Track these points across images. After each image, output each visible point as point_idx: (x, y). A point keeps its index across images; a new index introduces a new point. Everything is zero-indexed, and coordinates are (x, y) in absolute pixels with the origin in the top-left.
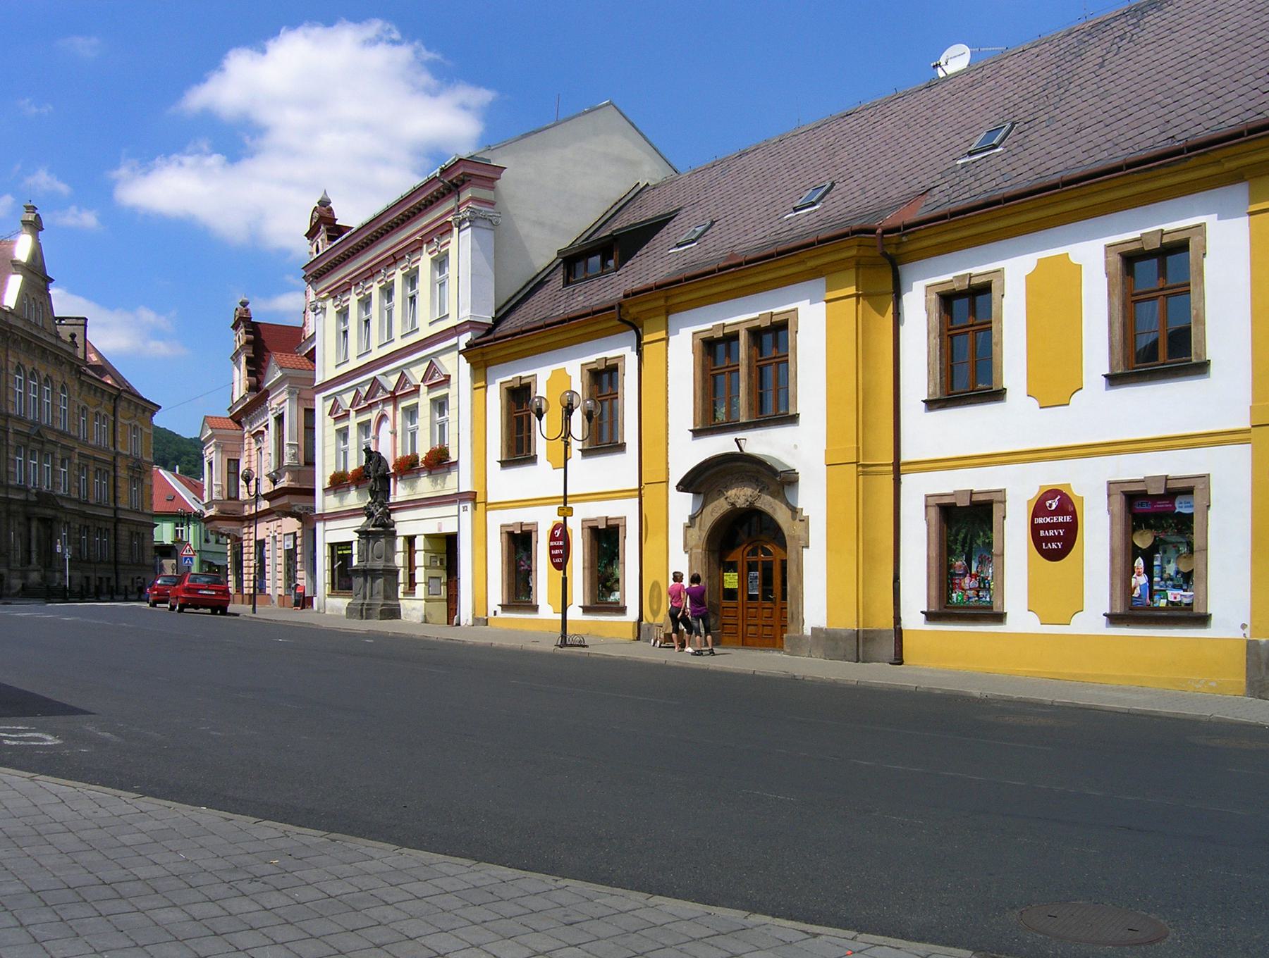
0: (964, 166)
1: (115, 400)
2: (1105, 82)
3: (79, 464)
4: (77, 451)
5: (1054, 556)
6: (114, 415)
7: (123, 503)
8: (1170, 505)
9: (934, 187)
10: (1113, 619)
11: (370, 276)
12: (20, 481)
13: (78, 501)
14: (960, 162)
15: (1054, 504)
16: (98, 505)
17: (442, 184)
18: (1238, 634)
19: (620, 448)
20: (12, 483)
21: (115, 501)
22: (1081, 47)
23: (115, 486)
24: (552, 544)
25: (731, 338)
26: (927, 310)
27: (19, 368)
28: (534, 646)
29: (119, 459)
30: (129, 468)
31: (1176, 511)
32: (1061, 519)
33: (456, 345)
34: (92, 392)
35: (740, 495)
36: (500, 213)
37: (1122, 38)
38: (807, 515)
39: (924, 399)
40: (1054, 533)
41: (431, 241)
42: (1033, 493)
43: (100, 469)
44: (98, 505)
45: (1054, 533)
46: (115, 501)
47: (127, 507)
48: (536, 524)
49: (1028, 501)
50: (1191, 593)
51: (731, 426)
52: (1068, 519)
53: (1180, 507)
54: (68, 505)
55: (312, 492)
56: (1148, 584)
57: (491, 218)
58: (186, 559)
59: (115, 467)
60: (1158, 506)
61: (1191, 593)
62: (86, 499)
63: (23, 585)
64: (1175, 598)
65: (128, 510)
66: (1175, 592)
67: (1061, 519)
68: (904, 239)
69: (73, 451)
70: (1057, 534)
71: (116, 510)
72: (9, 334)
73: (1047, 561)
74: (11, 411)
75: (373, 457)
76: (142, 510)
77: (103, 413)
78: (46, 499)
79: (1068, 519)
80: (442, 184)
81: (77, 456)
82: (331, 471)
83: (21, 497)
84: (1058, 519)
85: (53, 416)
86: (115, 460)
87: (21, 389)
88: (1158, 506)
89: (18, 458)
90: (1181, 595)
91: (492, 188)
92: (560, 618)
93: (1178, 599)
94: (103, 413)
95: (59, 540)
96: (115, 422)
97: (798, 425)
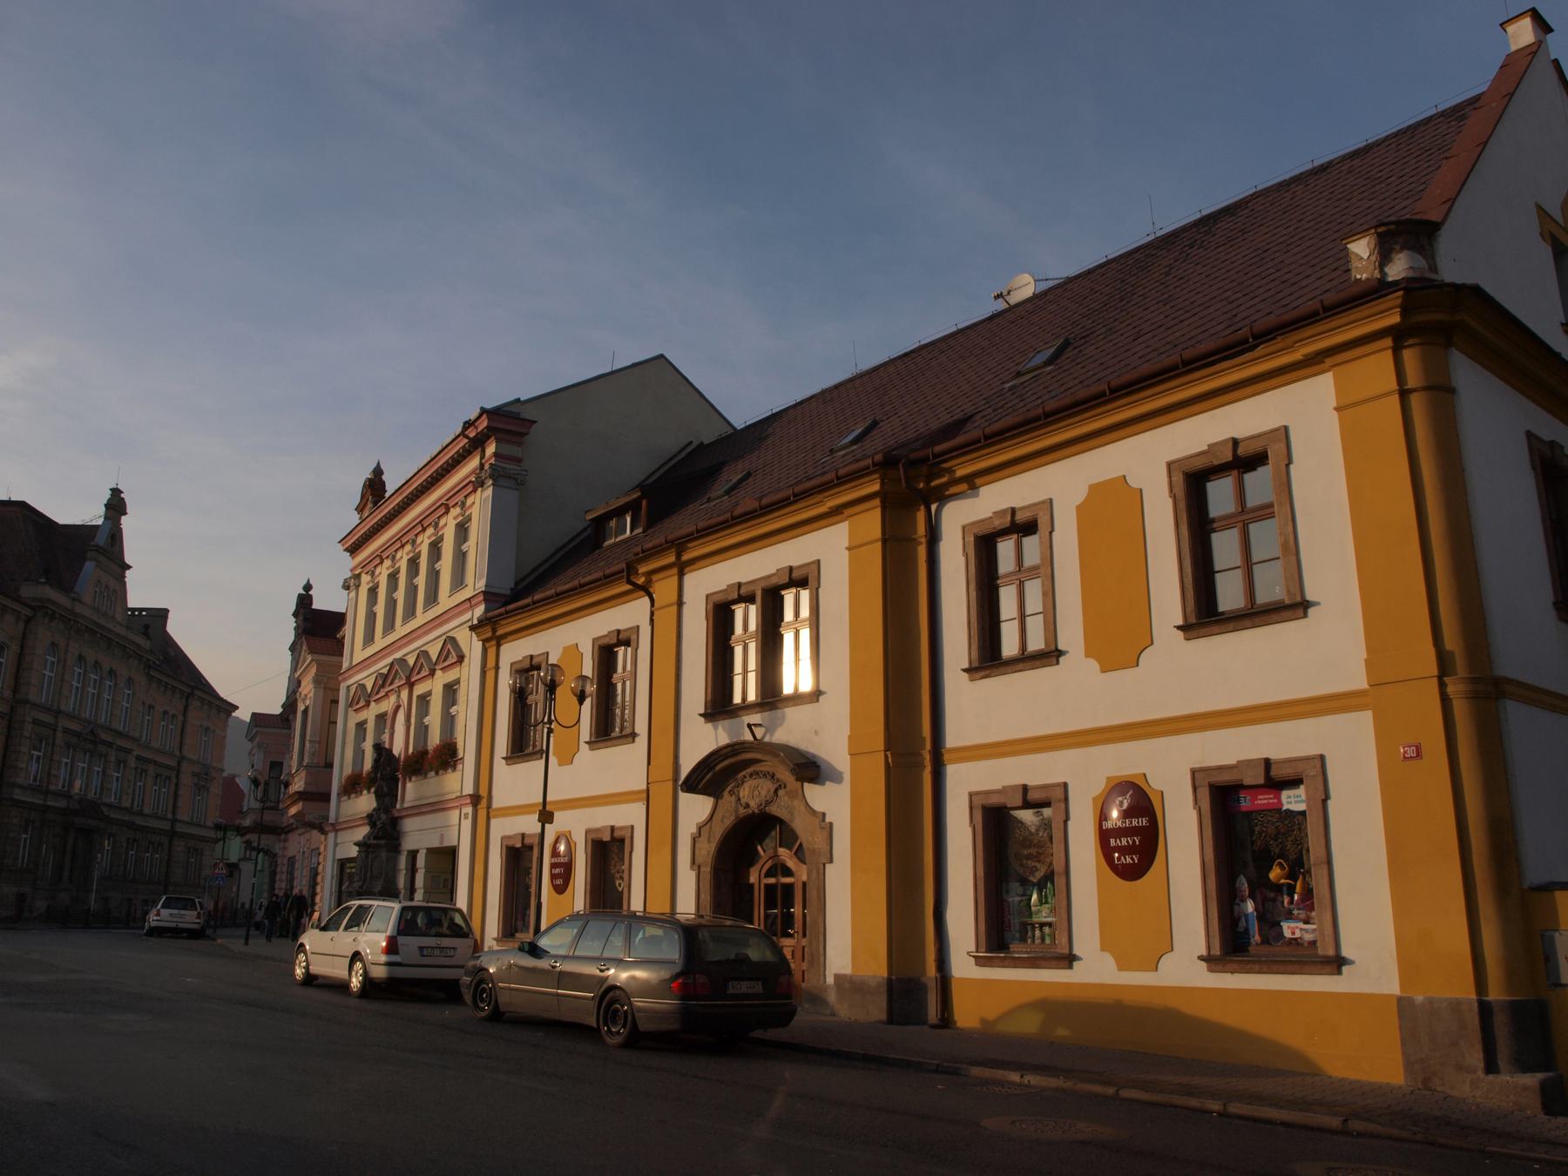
0: (1010, 389)
1: (187, 698)
2: (1171, 288)
3: (136, 768)
4: (135, 753)
5: (1131, 873)
6: (184, 715)
7: (183, 815)
8: (1275, 801)
9: (977, 413)
11: (400, 548)
12: (63, 787)
13: (129, 811)
14: (1007, 385)
15: (1125, 801)
16: (155, 816)
17: (466, 441)
18: (1391, 985)
19: (633, 736)
20: (52, 787)
21: (174, 813)
22: (1148, 260)
23: (176, 796)
26: (966, 554)
27: (81, 658)
29: (184, 765)
30: (195, 774)
31: (1284, 808)
34: (162, 689)
35: (752, 793)
36: (526, 471)
37: (1191, 246)
39: (964, 667)
43: (161, 775)
44: (155, 816)
45: (1128, 842)
46: (174, 813)
47: (186, 819)
49: (1094, 799)
50: (1314, 927)
52: (1143, 822)
53: (1288, 803)
54: (114, 815)
55: (326, 797)
56: (1255, 914)
57: (516, 476)
58: (217, 878)
59: (178, 772)
60: (1259, 802)
61: (1314, 927)
62: (139, 808)
63: (48, 906)
64: (1293, 933)
65: (188, 823)
66: (1293, 925)
69: (129, 753)
71: (174, 821)
72: (72, 623)
73: (1119, 879)
74: (63, 707)
75: (381, 751)
76: (205, 822)
77: (171, 713)
78: (90, 808)
79: (1143, 822)
80: (466, 441)
81: (134, 760)
82: (348, 771)
83: (62, 804)
84: (1131, 822)
85: (112, 714)
86: (179, 765)
87: (52, 672)
88: (1259, 802)
89: (65, 760)
90: (1301, 929)
91: (520, 444)
93: (1298, 935)
94: (171, 713)
95: (99, 855)
96: (184, 722)
97: (594, 640)
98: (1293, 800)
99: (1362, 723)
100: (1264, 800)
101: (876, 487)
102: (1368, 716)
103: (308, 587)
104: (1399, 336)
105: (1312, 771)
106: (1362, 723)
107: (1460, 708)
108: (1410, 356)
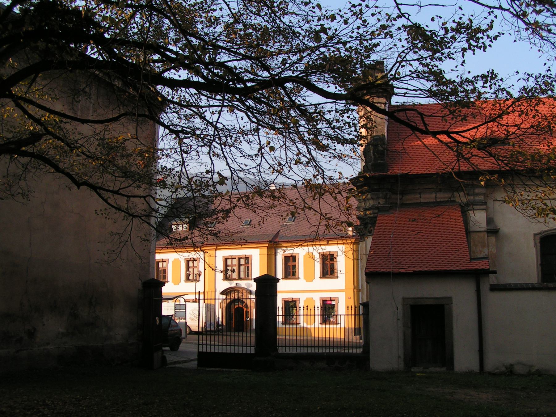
35: (235, 295)
98: (333, 303)
99: (343, 294)
100: (329, 302)
101: (267, 245)
102: (344, 293)
103: (474, 54)
104: (354, 243)
105: (336, 299)
106: (343, 294)
107: (356, 293)
108: (355, 246)
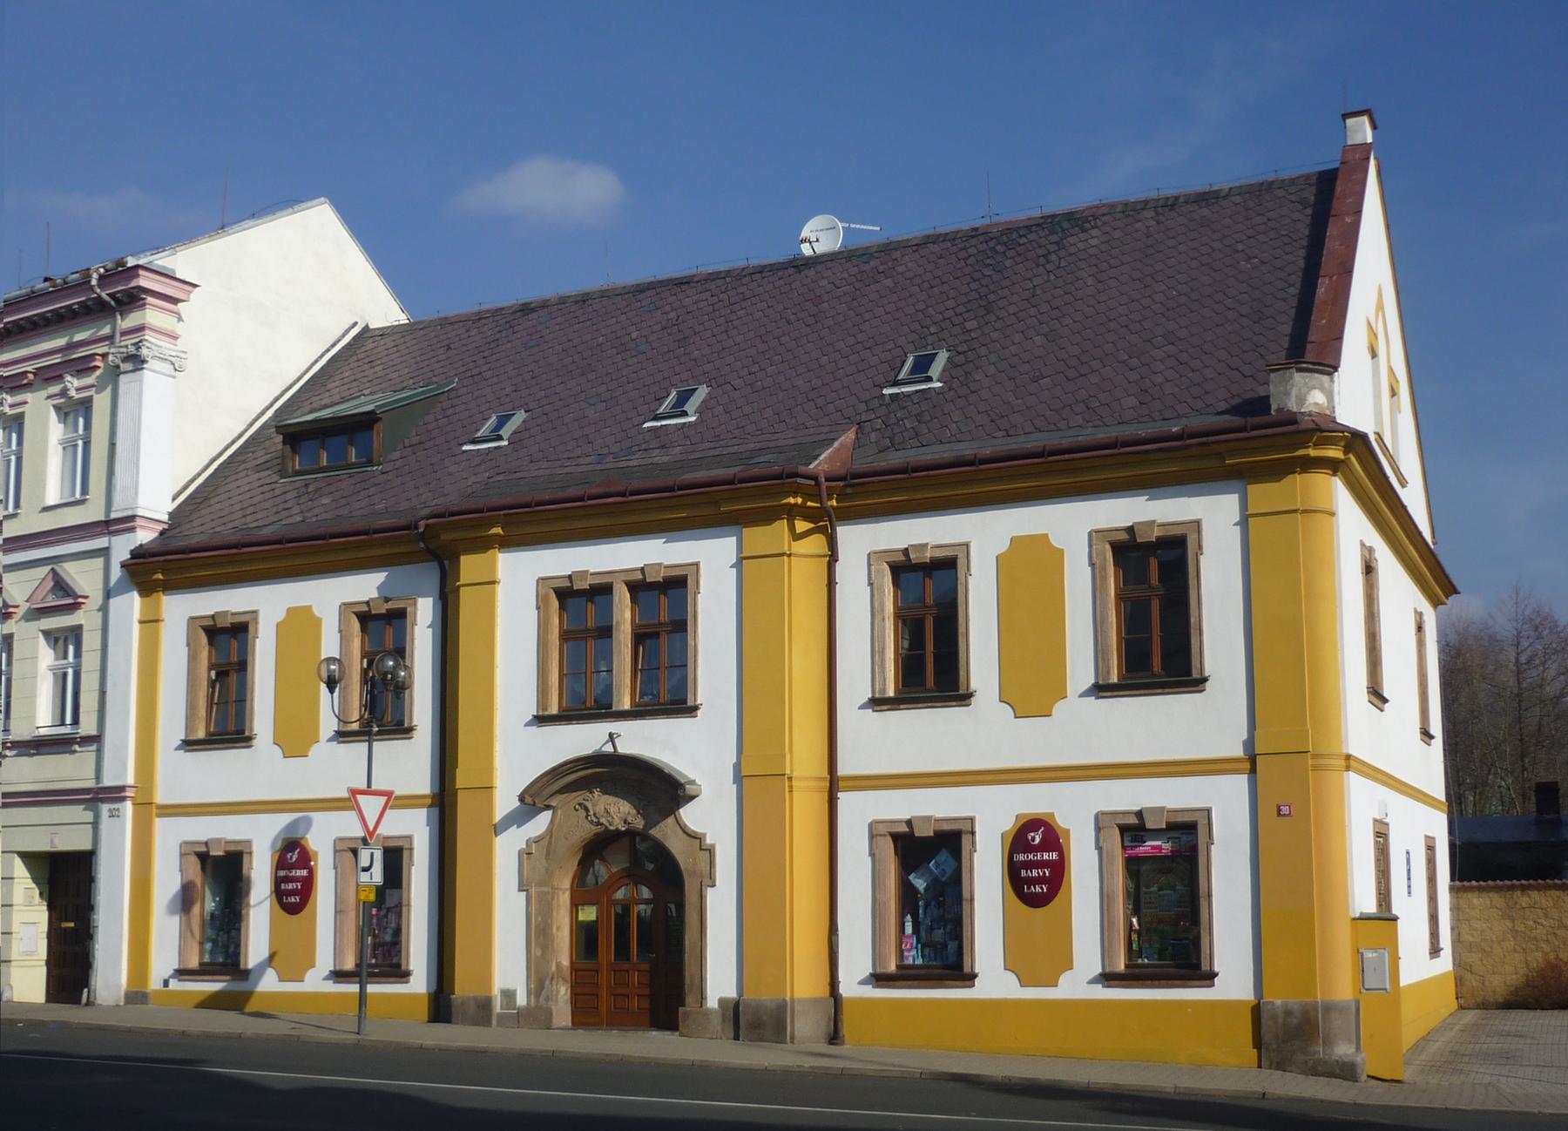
5: (293, 910)
10: (1108, 978)
24: (282, 873)
25: (601, 591)
28: (336, 1037)
32: (1046, 856)
33: (105, 552)
35: (617, 811)
38: (712, 842)
40: (1038, 873)
41: (58, 376)
42: (1008, 824)
45: (1038, 873)
48: (249, 842)
51: (601, 710)
52: (1054, 856)
67: (1046, 856)
68: (849, 490)
70: (1041, 874)
79: (1054, 856)
92: (358, 990)
